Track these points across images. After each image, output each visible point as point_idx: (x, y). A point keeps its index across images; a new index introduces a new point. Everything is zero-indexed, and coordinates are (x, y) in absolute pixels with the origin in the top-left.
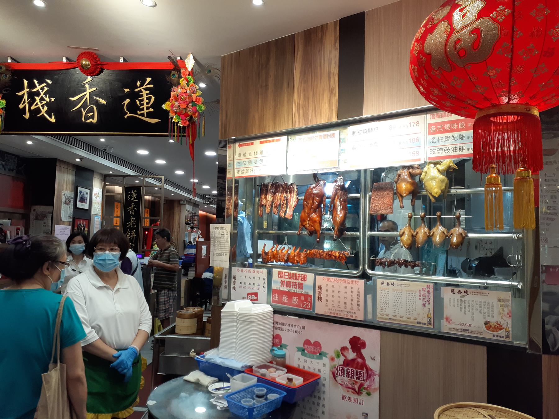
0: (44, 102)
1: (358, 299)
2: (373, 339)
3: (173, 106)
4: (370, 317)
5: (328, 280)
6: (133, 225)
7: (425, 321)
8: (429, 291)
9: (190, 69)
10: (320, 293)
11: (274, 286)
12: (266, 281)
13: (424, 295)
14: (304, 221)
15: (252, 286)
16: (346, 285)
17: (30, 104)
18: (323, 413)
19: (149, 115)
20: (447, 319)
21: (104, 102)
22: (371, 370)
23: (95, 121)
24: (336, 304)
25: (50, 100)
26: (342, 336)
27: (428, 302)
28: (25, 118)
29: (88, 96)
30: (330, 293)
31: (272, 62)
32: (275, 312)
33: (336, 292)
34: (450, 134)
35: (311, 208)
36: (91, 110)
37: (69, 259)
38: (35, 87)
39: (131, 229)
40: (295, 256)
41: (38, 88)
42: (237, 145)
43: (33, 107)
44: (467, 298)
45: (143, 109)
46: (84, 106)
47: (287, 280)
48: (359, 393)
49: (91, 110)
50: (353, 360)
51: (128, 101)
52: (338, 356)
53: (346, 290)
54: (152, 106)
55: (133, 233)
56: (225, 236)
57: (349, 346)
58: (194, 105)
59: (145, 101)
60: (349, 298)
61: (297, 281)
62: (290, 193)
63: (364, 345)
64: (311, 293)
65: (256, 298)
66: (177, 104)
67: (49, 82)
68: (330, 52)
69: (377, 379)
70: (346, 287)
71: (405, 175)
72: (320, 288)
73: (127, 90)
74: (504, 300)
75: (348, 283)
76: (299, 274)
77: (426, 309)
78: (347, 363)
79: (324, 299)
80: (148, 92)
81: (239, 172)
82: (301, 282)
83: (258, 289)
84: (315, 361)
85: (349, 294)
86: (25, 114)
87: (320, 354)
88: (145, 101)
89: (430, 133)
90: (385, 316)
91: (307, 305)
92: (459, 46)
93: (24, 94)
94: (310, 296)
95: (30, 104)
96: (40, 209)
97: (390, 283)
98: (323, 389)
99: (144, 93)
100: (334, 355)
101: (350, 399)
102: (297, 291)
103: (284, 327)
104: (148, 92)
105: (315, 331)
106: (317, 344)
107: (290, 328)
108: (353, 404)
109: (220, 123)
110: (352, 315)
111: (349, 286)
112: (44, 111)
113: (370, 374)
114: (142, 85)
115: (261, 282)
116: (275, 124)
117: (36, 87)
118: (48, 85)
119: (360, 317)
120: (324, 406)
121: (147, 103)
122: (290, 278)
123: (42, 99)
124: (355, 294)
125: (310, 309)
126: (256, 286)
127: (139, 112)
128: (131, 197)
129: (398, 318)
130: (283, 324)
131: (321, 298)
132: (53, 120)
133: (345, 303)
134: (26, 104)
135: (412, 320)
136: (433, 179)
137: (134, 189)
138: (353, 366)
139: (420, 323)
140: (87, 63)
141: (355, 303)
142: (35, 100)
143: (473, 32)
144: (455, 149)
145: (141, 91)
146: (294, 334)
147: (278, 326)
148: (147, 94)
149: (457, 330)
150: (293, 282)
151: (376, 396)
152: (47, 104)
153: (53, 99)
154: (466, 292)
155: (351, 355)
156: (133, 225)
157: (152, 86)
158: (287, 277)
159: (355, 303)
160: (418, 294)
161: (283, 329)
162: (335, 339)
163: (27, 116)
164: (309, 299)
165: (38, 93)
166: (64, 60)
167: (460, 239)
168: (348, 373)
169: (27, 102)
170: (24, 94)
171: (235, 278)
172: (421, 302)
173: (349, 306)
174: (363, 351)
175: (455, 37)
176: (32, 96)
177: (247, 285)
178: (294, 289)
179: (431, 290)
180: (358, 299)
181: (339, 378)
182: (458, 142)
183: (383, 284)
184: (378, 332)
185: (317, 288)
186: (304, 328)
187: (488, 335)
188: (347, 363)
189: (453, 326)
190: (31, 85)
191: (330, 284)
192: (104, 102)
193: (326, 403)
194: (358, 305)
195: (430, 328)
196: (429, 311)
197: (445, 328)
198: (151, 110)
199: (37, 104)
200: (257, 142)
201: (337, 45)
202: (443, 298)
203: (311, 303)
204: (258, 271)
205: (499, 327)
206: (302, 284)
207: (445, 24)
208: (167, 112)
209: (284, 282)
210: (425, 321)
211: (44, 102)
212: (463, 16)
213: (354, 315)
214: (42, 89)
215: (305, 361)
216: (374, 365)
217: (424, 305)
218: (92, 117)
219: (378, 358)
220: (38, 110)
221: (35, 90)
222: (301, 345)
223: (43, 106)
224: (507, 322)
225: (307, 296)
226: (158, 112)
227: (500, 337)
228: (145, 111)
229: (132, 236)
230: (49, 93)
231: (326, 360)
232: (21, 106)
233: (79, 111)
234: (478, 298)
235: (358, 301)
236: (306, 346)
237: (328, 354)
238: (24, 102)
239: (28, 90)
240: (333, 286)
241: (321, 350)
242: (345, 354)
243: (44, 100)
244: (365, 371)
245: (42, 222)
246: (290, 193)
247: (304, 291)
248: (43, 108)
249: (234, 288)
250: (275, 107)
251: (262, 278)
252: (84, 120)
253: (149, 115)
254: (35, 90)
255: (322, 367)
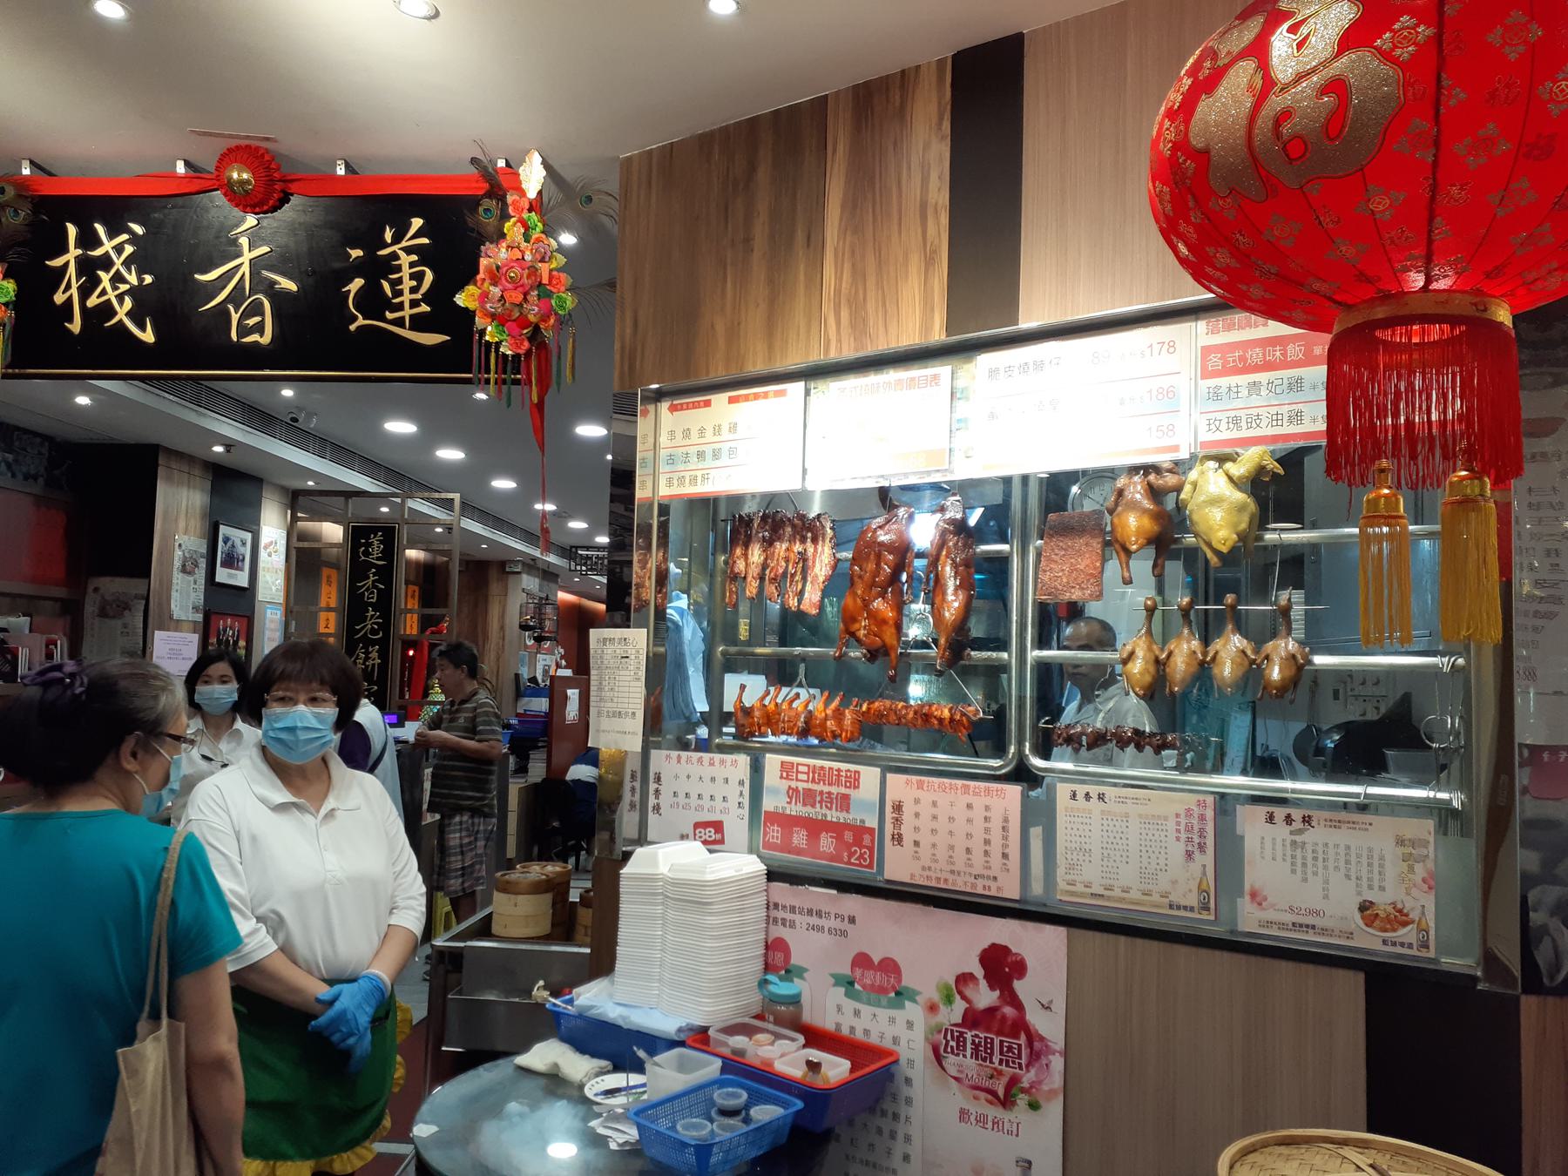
0: (124, 287)
1: (1005, 838)
2: (1045, 951)
3: (484, 297)
4: (1037, 889)
5: (920, 786)
6: (374, 632)
7: (1193, 900)
8: (1202, 818)
9: (532, 194)
10: (897, 822)
11: (769, 804)
12: (746, 790)
13: (1189, 829)
14: (854, 620)
15: (706, 802)
16: (969, 799)
17: (85, 293)
18: (906, 1158)
19: (419, 323)
20: (1253, 895)
21: (293, 287)
22: (1042, 1039)
23: (266, 339)
24: (942, 853)
25: (141, 280)
26: (958, 943)
27: (1202, 847)
28: (69, 331)
29: (246, 269)
30: (925, 823)
31: (763, 174)
32: (772, 876)
33: (943, 819)
34: (1263, 377)
35: (873, 584)
36: (256, 309)
37: (193, 726)
38: (98, 243)
39: (368, 643)
40: (826, 718)
41: (108, 246)
42: (664, 406)
43: (93, 301)
44: (1310, 836)
45: (400, 307)
46: (236, 297)
47: (805, 785)
48: (1007, 1102)
49: (256, 309)
50: (991, 1011)
51: (358, 283)
52: (949, 1000)
53: (970, 814)
54: (427, 298)
55: (374, 655)
56: (632, 661)
57: (979, 972)
58: (545, 295)
59: (408, 284)
60: (979, 836)
61: (834, 790)
62: (815, 541)
63: (1020, 968)
64: (872, 822)
65: (718, 836)
66: (496, 291)
67: (138, 229)
68: (927, 146)
69: (1057, 1063)
70: (969, 806)
71: (1136, 490)
72: (898, 808)
73: (356, 253)
74: (1413, 843)
75: (976, 794)
76: (839, 770)
77: (1195, 867)
78: (973, 1019)
79: (908, 838)
80: (414, 258)
81: (670, 482)
82: (843, 790)
83: (724, 811)
84: (884, 1014)
85: (979, 824)
86: (71, 320)
87: (898, 993)
88: (408, 284)
89: (1206, 374)
90: (1080, 888)
91: (862, 856)
92: (1286, 129)
93: (67, 264)
94: (871, 831)
95: (85, 293)
96: (113, 586)
97: (1094, 795)
98: (905, 1091)
99: (405, 260)
100: (936, 997)
101: (981, 1120)
102: (833, 815)
103: (797, 918)
104: (414, 258)
105: (885, 930)
106: (890, 967)
107: (814, 920)
108: (990, 1135)
109: (617, 346)
110: (987, 883)
111: (980, 803)
112: (123, 310)
113: (1037, 1049)
114: (397, 239)
115: (733, 791)
116: (770, 347)
117: (100, 244)
118: (134, 239)
119: (1010, 889)
120: (908, 1139)
121: (413, 290)
122: (813, 781)
123: (118, 279)
124: (996, 825)
125: (870, 866)
126: (718, 802)
127: (389, 315)
128: (367, 553)
129: (1117, 893)
130: (793, 909)
131: (900, 835)
132: (148, 336)
133: (968, 851)
134: (74, 291)
135: (1156, 898)
136: (1215, 501)
137: (375, 530)
138: (991, 1026)
139: (1179, 908)
140: (245, 176)
141: (996, 850)
142: (99, 281)
143: (1326, 89)
144: (1276, 419)
145: (395, 256)
146: (823, 937)
147: (780, 914)
148: (412, 265)
149: (1282, 926)
150: (821, 793)
151: (1053, 1111)
152: (132, 292)
153: (148, 279)
154: (1307, 820)
155: (985, 997)
156: (374, 632)
157: (425, 241)
158: (804, 777)
159: (996, 850)
160: (1171, 825)
161: (792, 925)
162: (940, 951)
163: (76, 326)
164: (867, 839)
165: (106, 262)
166: (180, 168)
167: (1290, 672)
168: (976, 1047)
169: (74, 285)
170: (67, 264)
171: (658, 779)
172: (1181, 848)
173: (978, 858)
174: (1018, 985)
175: (1276, 102)
176: (90, 269)
177: (694, 801)
178: (824, 811)
179: (1210, 814)
180: (1005, 838)
181: (951, 1061)
182: (1285, 399)
183: (1074, 796)
184: (1061, 931)
185: (889, 809)
186: (852, 920)
187: (1370, 941)
188: (973, 1019)
189: (1271, 915)
190: (88, 240)
191: (926, 797)
192: (293, 287)
193: (915, 1130)
194: (1005, 856)
195: (1205, 922)
196: (1204, 873)
197: (1249, 920)
198: (425, 308)
199: (104, 292)
200: (720, 399)
201: (947, 125)
202: (1242, 838)
203: (871, 849)
204: (722, 762)
205: (1400, 918)
206: (846, 797)
207: (1247, 67)
208: (468, 315)
209: (796, 790)
210: (1193, 900)
211: (124, 287)
212: (1300, 46)
213: (994, 885)
214: (119, 249)
215: (857, 1013)
216: (1049, 1025)
217: (1189, 855)
218: (259, 328)
219: (1060, 1006)
220: (107, 310)
221: (98, 252)
222: (845, 970)
223: (120, 298)
224: (1422, 905)
225: (860, 831)
226: (443, 313)
227: (1403, 945)
228: (407, 312)
229: (370, 663)
230: (138, 261)
231: (913, 1011)
232: (59, 298)
233: (222, 313)
234: (1341, 837)
235: (1005, 846)
236: (858, 972)
237: (919, 993)
238: (68, 287)
239: (80, 252)
240: (934, 804)
241: (900, 981)
242: (968, 992)
243: (125, 281)
244: (1023, 1040)
245: (119, 623)
246: (815, 541)
247: (853, 816)
248: (121, 302)
249: (657, 808)
250: (772, 301)
251: (734, 782)
252: (234, 338)
253: (419, 323)
254: (98, 252)
255: (903, 1031)
